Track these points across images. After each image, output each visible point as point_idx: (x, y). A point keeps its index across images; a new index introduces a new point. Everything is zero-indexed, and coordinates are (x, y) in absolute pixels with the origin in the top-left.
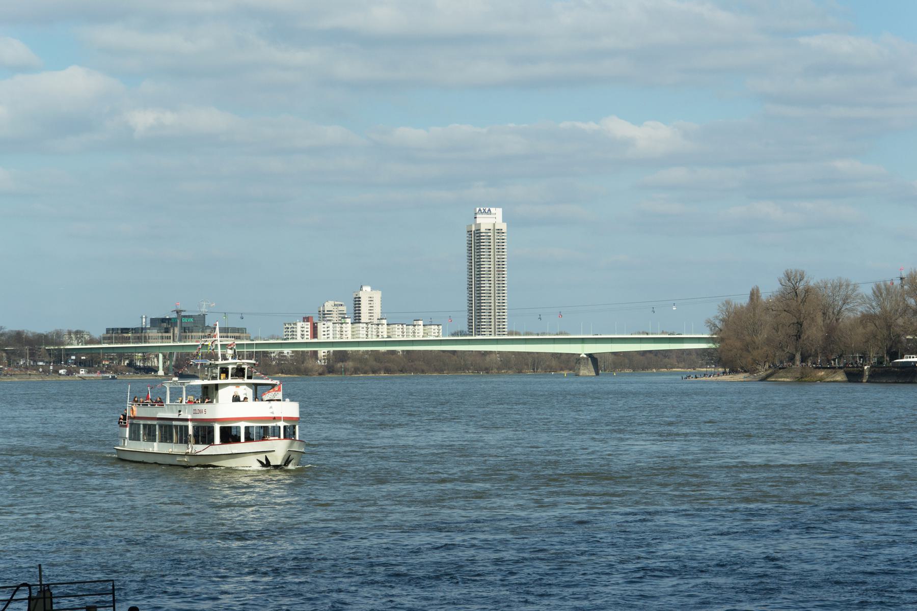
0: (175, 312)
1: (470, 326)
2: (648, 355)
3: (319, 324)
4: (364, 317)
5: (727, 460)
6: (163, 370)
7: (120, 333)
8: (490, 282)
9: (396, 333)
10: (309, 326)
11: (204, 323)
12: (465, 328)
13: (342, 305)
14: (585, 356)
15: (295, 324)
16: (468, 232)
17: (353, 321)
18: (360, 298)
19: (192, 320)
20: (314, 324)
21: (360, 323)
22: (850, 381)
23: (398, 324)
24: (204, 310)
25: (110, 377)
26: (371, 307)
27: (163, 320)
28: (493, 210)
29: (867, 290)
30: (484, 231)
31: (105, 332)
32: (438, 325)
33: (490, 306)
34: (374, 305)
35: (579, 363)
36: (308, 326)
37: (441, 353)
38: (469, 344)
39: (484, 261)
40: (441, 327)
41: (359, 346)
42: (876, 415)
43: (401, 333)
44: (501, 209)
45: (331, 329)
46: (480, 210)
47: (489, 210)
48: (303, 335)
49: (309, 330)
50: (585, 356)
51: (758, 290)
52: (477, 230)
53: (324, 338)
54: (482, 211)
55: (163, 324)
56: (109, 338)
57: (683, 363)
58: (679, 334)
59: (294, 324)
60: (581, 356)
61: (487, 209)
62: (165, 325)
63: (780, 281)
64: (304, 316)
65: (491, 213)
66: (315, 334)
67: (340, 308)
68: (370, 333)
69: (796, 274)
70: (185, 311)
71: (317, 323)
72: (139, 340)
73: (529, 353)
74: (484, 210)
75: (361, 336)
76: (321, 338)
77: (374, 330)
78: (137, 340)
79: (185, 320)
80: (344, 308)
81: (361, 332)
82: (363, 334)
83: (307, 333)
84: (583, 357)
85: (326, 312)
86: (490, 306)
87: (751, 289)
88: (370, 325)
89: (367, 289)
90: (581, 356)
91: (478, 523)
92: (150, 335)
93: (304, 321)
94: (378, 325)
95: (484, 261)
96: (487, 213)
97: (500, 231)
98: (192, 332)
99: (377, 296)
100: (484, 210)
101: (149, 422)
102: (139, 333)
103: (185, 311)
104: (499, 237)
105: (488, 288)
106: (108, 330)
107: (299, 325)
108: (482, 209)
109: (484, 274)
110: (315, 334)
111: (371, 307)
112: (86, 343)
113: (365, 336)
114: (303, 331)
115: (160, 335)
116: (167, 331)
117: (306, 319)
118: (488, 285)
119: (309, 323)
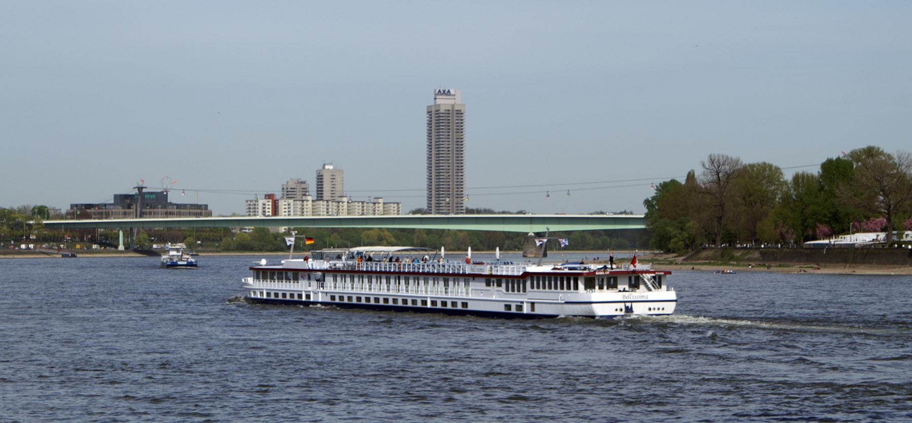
0: (137, 189)
1: (429, 205)
2: (396, 231)
3: (280, 201)
4: (327, 195)
5: (501, 336)
6: (124, 245)
7: (84, 210)
9: (357, 211)
10: (270, 203)
11: (167, 199)
12: (425, 206)
14: (533, 234)
16: (428, 112)
17: (315, 198)
18: (322, 176)
20: (275, 201)
21: (322, 200)
22: (764, 260)
23: (394, 203)
25: (70, 255)
26: (333, 185)
27: (126, 197)
29: (788, 176)
30: (444, 112)
31: (69, 208)
33: (449, 185)
34: (336, 183)
35: (528, 241)
36: (269, 204)
37: (589, 236)
42: (35, 288)
43: (325, 210)
47: (449, 91)
49: (270, 207)
50: (533, 234)
51: (694, 175)
52: (437, 111)
53: (285, 215)
55: (125, 201)
56: (73, 214)
57: (339, 237)
58: (562, 214)
60: (529, 234)
62: (128, 201)
63: (704, 165)
64: (266, 193)
65: (450, 95)
66: (275, 211)
68: (330, 210)
69: (719, 158)
70: (146, 188)
71: (278, 200)
72: (100, 215)
73: (504, 232)
74: (444, 91)
75: (322, 213)
76: (283, 215)
77: (335, 208)
78: (100, 216)
79: (147, 196)
81: (322, 210)
82: (323, 212)
84: (531, 236)
85: (289, 190)
86: (449, 185)
87: (687, 173)
88: (330, 203)
90: (529, 234)
91: (277, 400)
92: (113, 210)
93: (265, 198)
94: (339, 202)
98: (155, 208)
101: (367, 296)
102: (101, 209)
103: (146, 188)
105: (447, 168)
106: (72, 206)
107: (261, 202)
109: (443, 154)
110: (275, 211)
111: (333, 185)
112: (78, 218)
113: (325, 213)
115: (123, 210)
116: (129, 208)
119: (271, 200)
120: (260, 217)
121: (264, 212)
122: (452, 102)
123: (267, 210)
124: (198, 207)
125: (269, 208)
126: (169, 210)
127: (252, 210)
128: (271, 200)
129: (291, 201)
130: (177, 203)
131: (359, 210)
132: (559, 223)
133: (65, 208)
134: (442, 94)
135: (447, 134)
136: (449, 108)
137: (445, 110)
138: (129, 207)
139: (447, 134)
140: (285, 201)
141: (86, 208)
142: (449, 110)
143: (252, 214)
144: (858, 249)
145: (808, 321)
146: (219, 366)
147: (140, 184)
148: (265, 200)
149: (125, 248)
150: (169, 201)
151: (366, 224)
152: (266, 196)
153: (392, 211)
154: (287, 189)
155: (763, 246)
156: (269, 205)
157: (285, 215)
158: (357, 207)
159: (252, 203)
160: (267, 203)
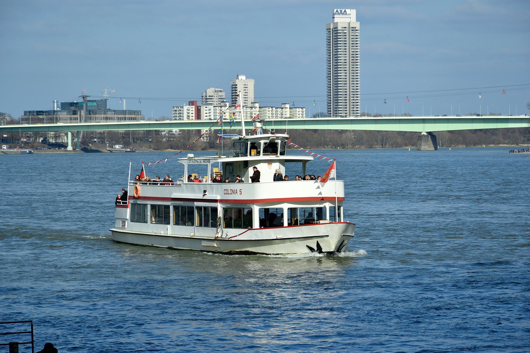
8: (345, 72)
10: (194, 109)
11: (106, 106)
12: (325, 111)
13: (221, 91)
14: (426, 134)
15: (182, 107)
19: (95, 104)
20: (198, 107)
24: (106, 95)
26: (245, 93)
28: (348, 11)
31: (23, 114)
32: (302, 108)
36: (193, 109)
38: (328, 124)
39: (341, 54)
40: (304, 109)
41: (192, 127)
44: (355, 10)
45: (212, 111)
46: (337, 11)
47: (345, 11)
48: (188, 116)
49: (194, 112)
50: (426, 134)
52: (335, 28)
53: (299, 117)
54: (339, 12)
59: (181, 107)
61: (343, 10)
62: (73, 108)
64: (190, 100)
67: (220, 94)
70: (89, 96)
71: (200, 107)
74: (341, 11)
76: (204, 119)
80: (223, 94)
83: (192, 115)
84: (424, 135)
85: (208, 97)
89: (242, 77)
92: (61, 116)
93: (189, 105)
95: (341, 54)
96: (343, 14)
97: (354, 29)
99: (251, 84)
100: (341, 11)
102: (51, 115)
103: (89, 96)
104: (353, 34)
105: (344, 77)
107: (186, 108)
108: (339, 10)
111: (245, 93)
114: (188, 113)
115: (69, 116)
117: (191, 103)
118: (344, 74)
119: (194, 107)
120: (186, 121)
121: (188, 116)
122: (348, 20)
123: (191, 115)
124: (134, 112)
125: (192, 113)
126: (108, 116)
127: (178, 115)
128: (194, 107)
129: (211, 107)
130: (47, 110)
131: (269, 114)
132: (521, 122)
133: (18, 115)
134: (339, 14)
135: (344, 48)
136: (347, 26)
137: (342, 27)
138: (75, 113)
139: (344, 48)
140: (206, 107)
141: (37, 114)
142: (346, 28)
143: (177, 118)
144: (253, 176)
145: (328, 271)
146: (50, 264)
147: (85, 94)
148: (189, 106)
149: (73, 149)
150: (108, 108)
151: (139, 128)
152: (189, 102)
153: (297, 115)
154: (206, 96)
155: (450, 149)
156: (192, 111)
157: (299, 117)
158: (297, 112)
159: (178, 109)
160: (191, 109)
